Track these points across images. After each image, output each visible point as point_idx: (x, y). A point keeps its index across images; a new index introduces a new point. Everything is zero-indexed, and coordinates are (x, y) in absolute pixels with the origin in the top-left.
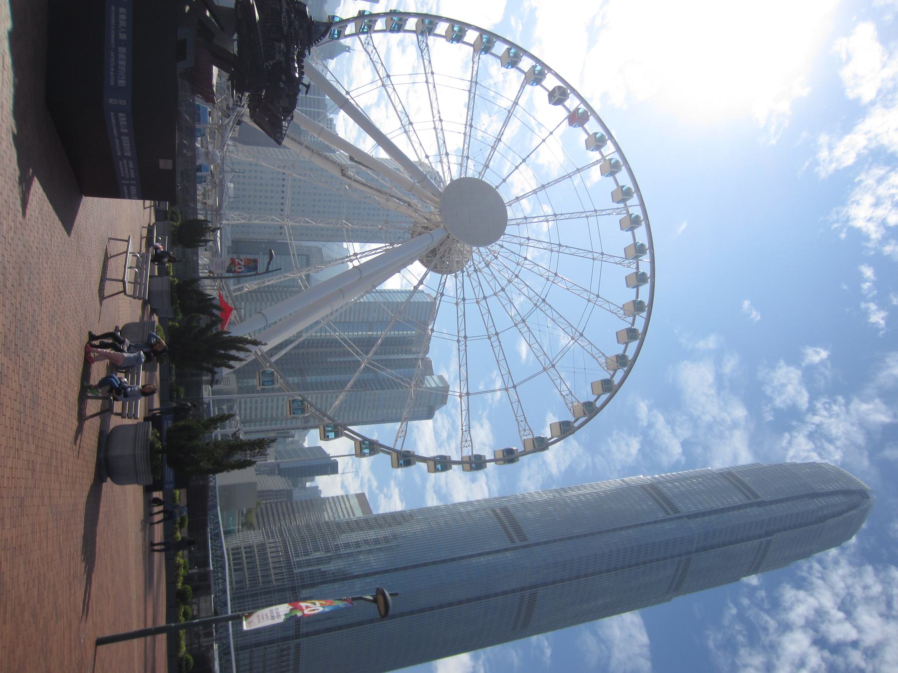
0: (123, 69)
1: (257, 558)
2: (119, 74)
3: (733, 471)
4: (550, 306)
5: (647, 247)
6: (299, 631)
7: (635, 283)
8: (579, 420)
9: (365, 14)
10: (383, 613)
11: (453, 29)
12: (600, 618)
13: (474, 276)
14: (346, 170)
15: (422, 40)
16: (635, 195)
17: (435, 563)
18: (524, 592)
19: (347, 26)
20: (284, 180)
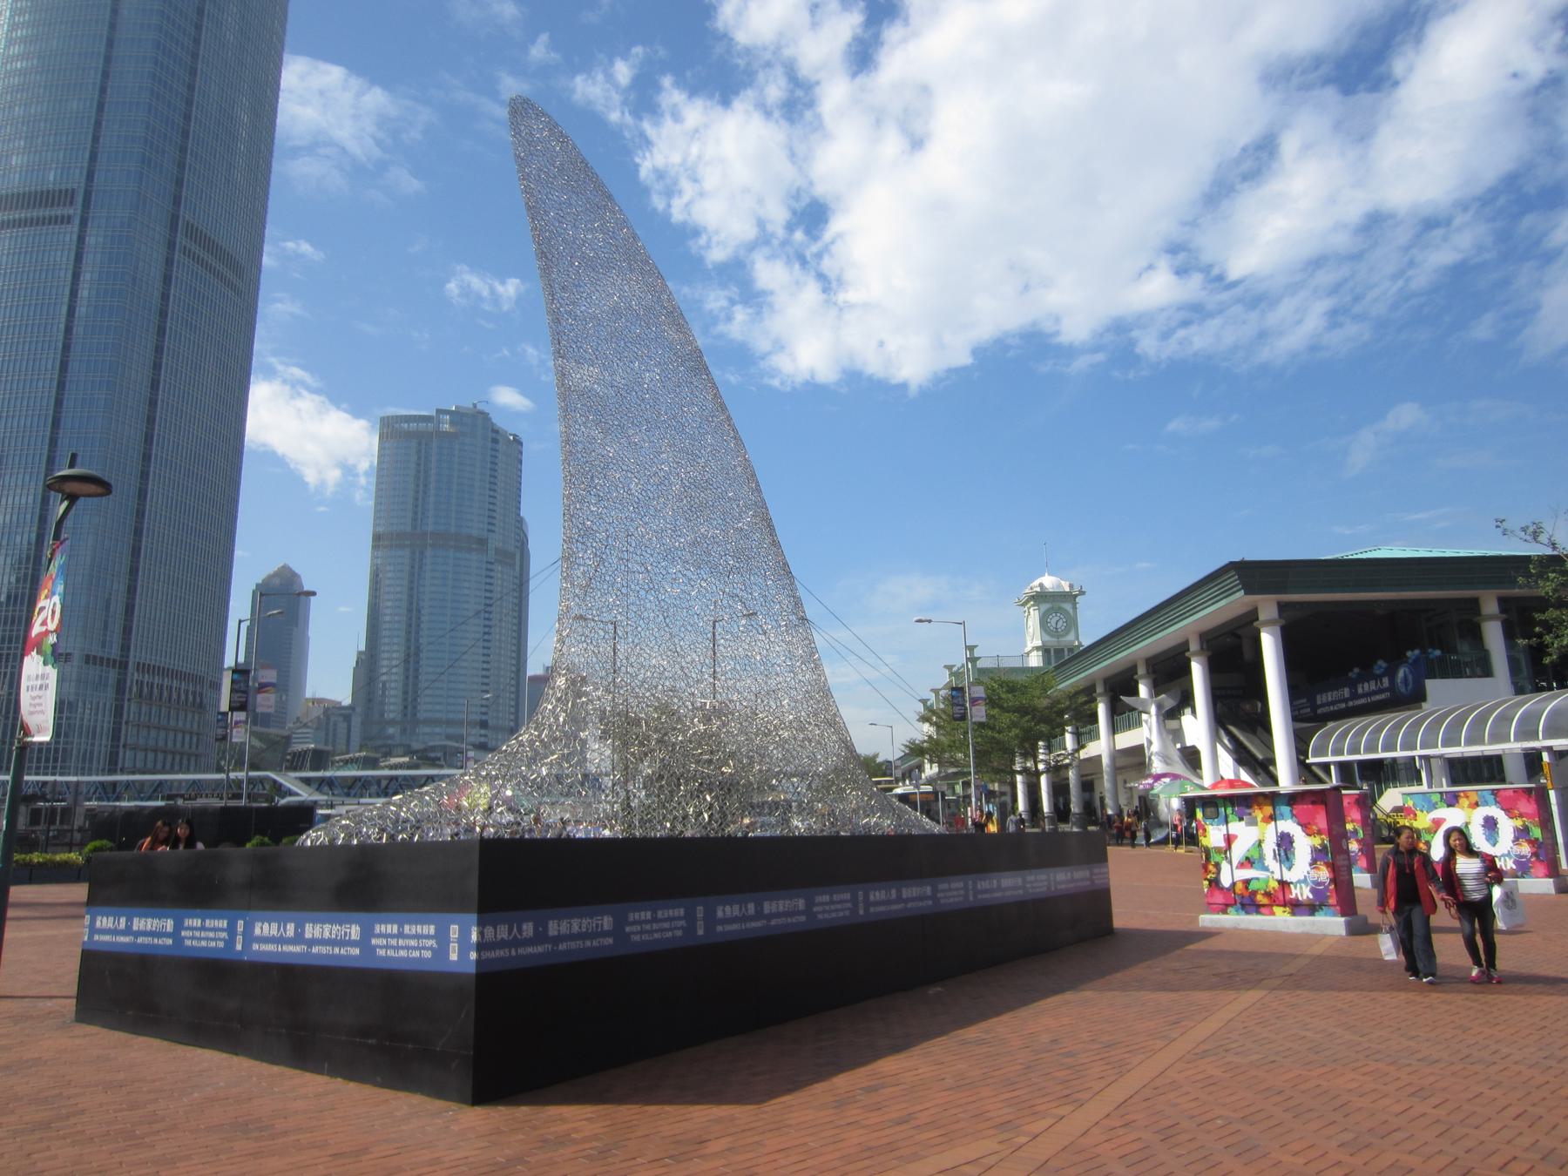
2: (595, 929)
10: (100, 490)
12: (274, 134)
17: (61, 386)
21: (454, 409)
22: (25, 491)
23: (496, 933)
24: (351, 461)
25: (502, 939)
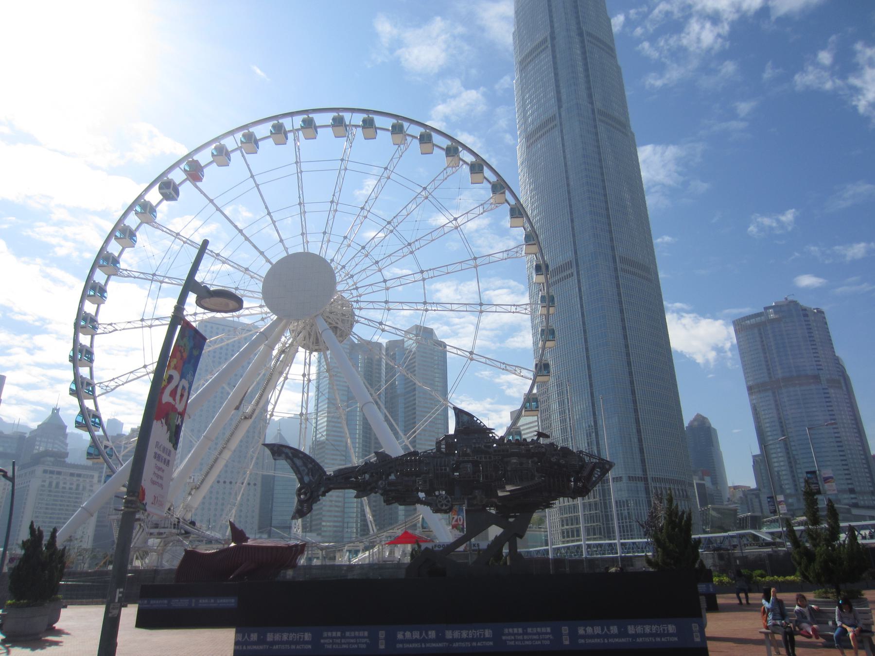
0: (654, 628)
1: (573, 515)
3: (519, 59)
4: (394, 217)
5: (306, 116)
6: (641, 477)
7: (372, 130)
8: (508, 199)
9: (74, 388)
11: (92, 296)
13: (361, 291)
14: (245, 414)
15: (103, 329)
16: (281, 121)
18: (618, 268)
19: (87, 408)
20: (225, 482)
21: (774, 304)
22: (576, 394)
23: (593, 630)
24: (720, 345)
25: (598, 633)
